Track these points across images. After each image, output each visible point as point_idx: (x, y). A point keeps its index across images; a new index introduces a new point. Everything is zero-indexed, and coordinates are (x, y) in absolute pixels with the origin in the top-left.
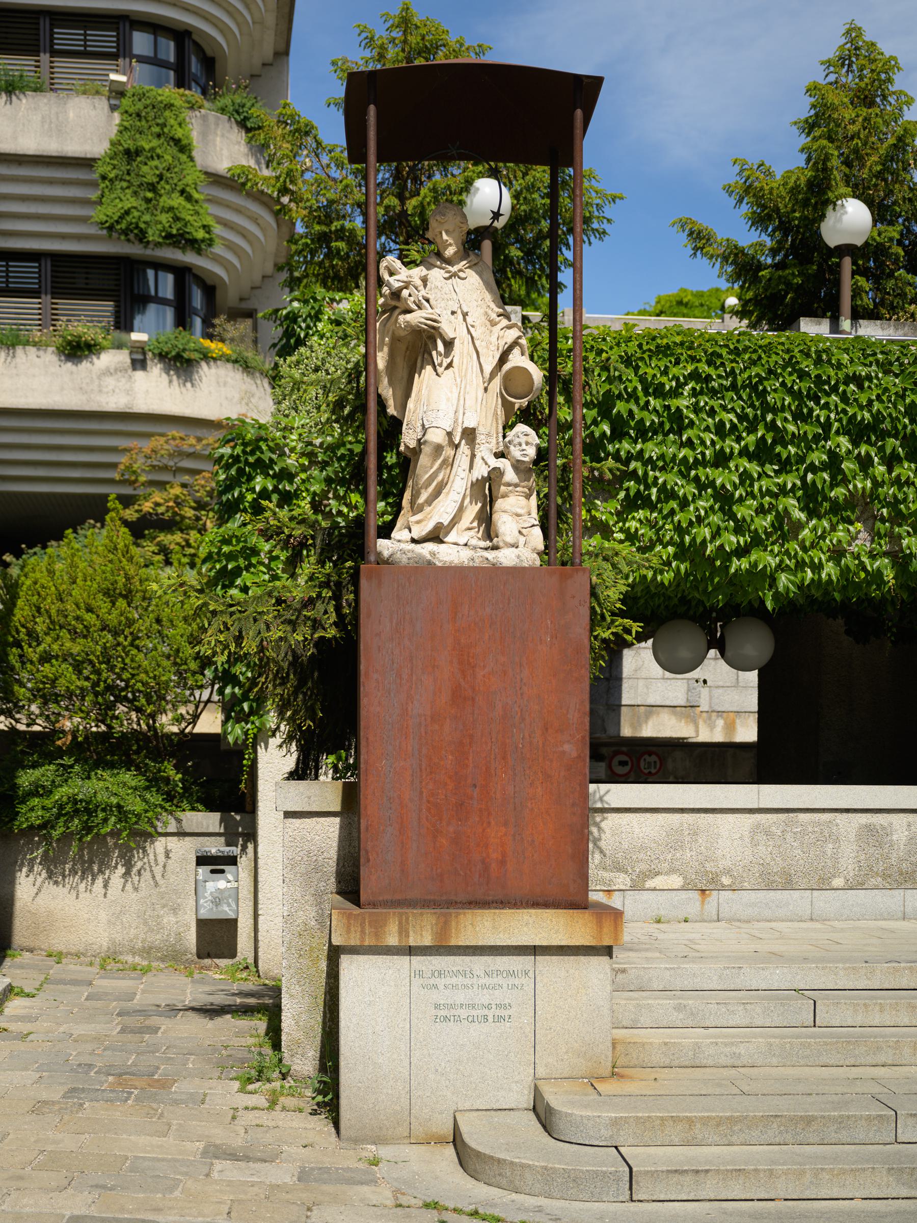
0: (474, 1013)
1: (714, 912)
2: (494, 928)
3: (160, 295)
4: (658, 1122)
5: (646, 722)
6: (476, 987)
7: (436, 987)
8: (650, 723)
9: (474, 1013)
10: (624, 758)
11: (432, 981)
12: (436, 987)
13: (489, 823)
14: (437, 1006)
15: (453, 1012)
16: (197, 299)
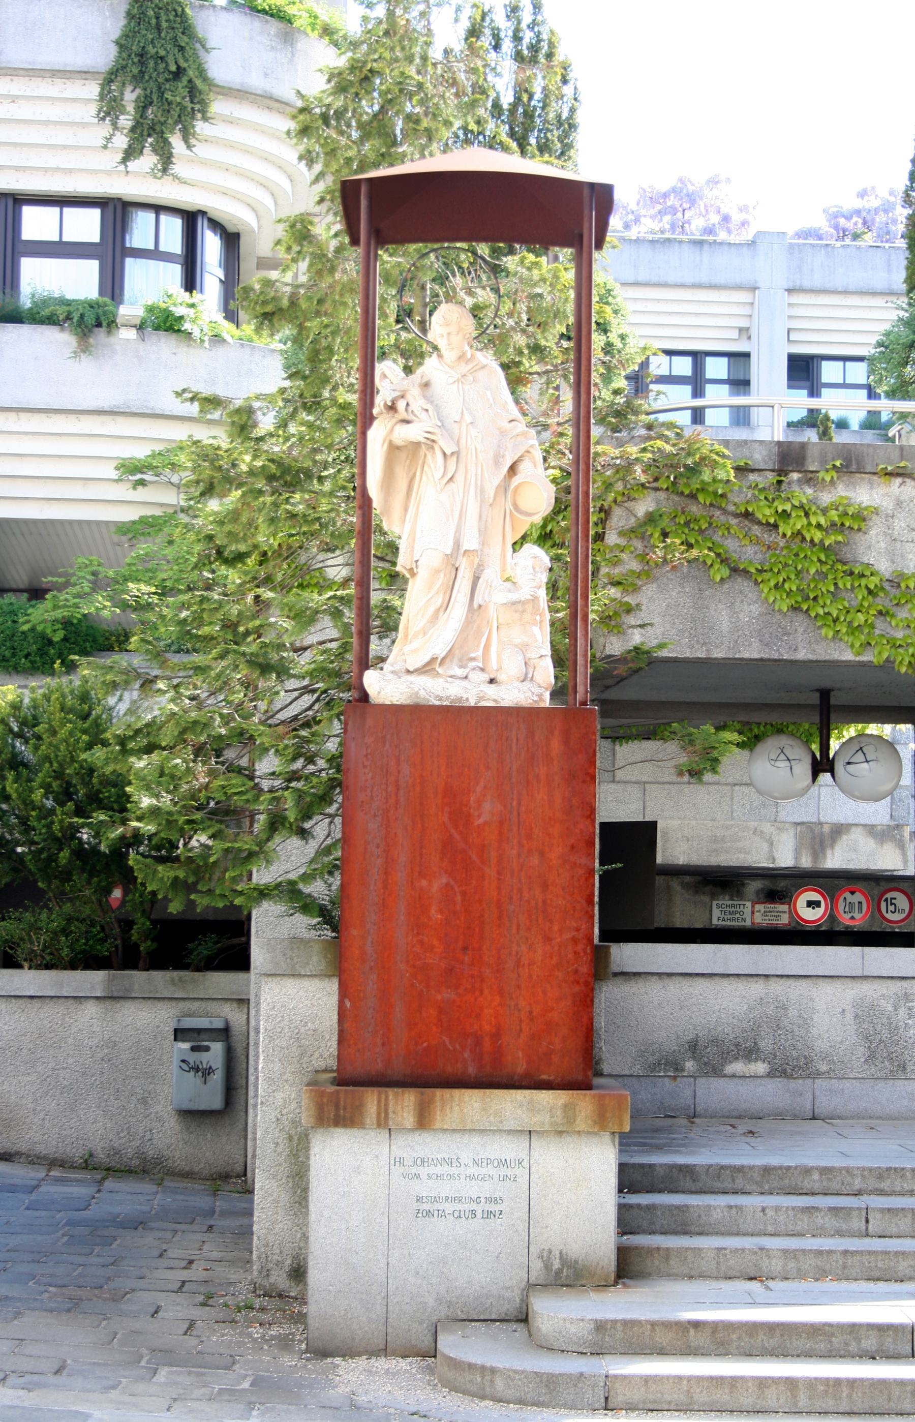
0: (459, 1207)
1: (809, 1106)
2: (484, 1109)
3: (162, 248)
4: (649, 1327)
5: (832, 848)
6: (463, 1177)
7: (417, 1176)
8: (838, 848)
9: (459, 1207)
10: (815, 896)
11: (414, 1170)
12: (417, 1176)
13: (481, 991)
14: (419, 1199)
15: (437, 1206)
16: (211, 246)
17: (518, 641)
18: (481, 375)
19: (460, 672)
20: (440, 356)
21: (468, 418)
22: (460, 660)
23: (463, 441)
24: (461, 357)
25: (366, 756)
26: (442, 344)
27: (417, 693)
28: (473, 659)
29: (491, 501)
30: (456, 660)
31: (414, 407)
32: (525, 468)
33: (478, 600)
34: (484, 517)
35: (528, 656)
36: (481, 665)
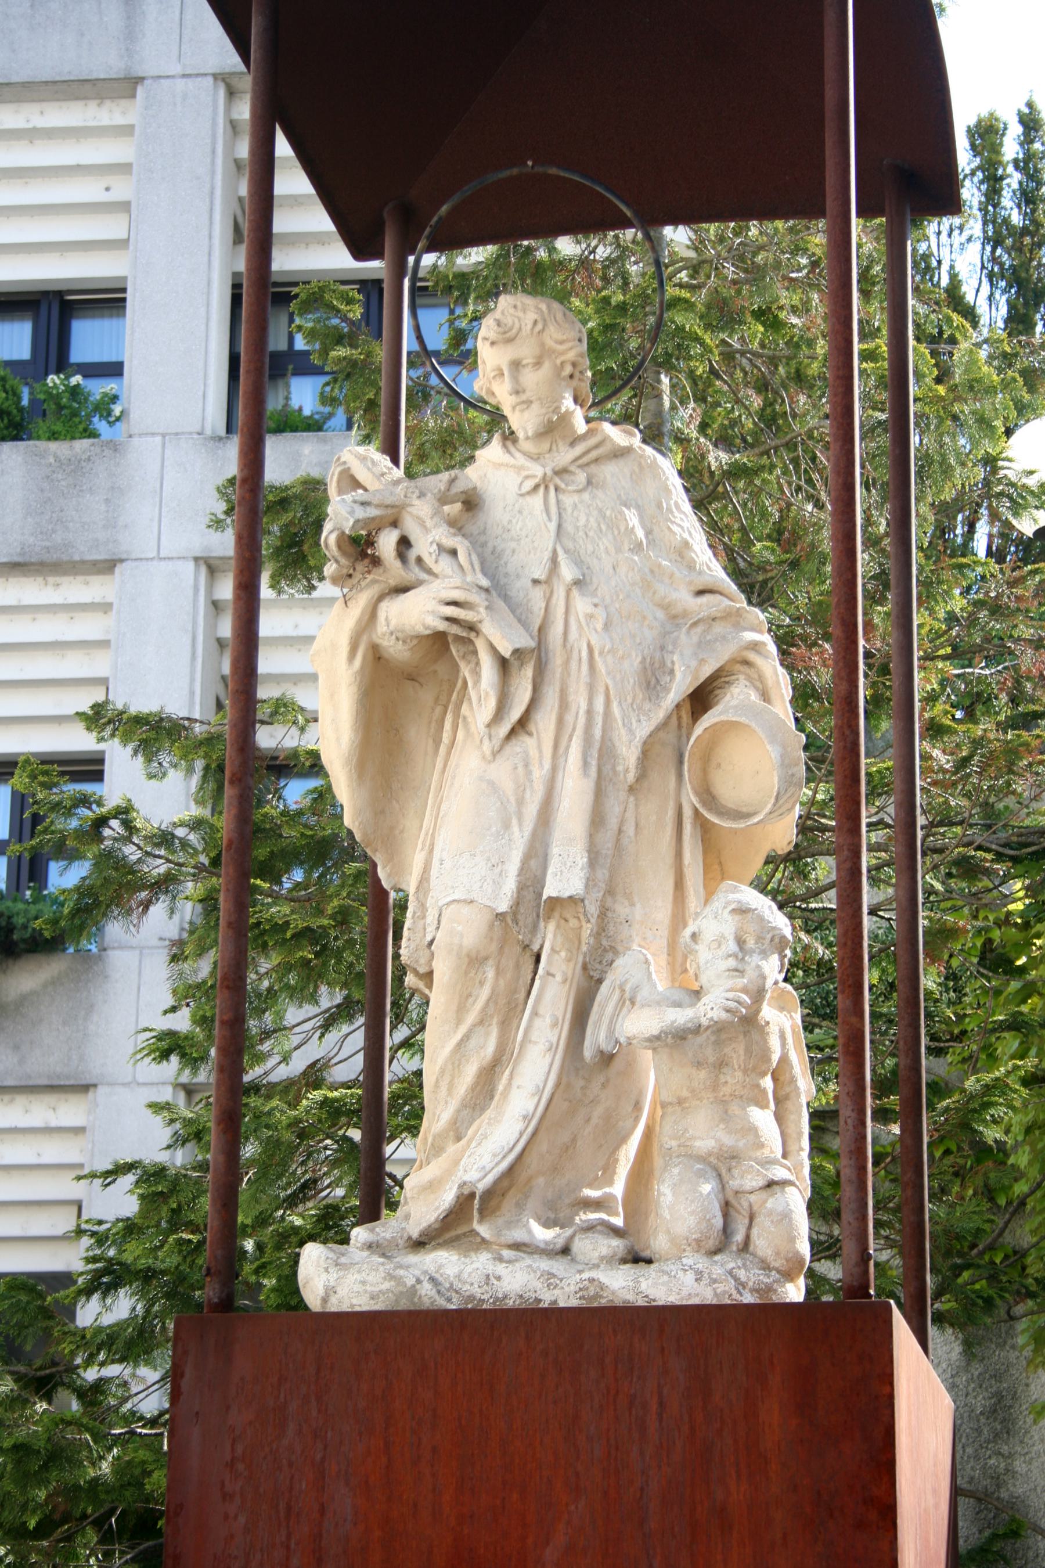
17: (705, 1144)
18: (609, 471)
19: (542, 1234)
20: (510, 437)
21: (567, 572)
22: (552, 1205)
23: (557, 629)
24: (554, 428)
25: (231, 1465)
26: (502, 395)
27: (413, 1291)
28: (596, 1205)
29: (631, 777)
30: (533, 1203)
31: (423, 546)
32: (735, 701)
33: (597, 1037)
34: (613, 822)
35: (734, 1184)
36: (618, 1221)
